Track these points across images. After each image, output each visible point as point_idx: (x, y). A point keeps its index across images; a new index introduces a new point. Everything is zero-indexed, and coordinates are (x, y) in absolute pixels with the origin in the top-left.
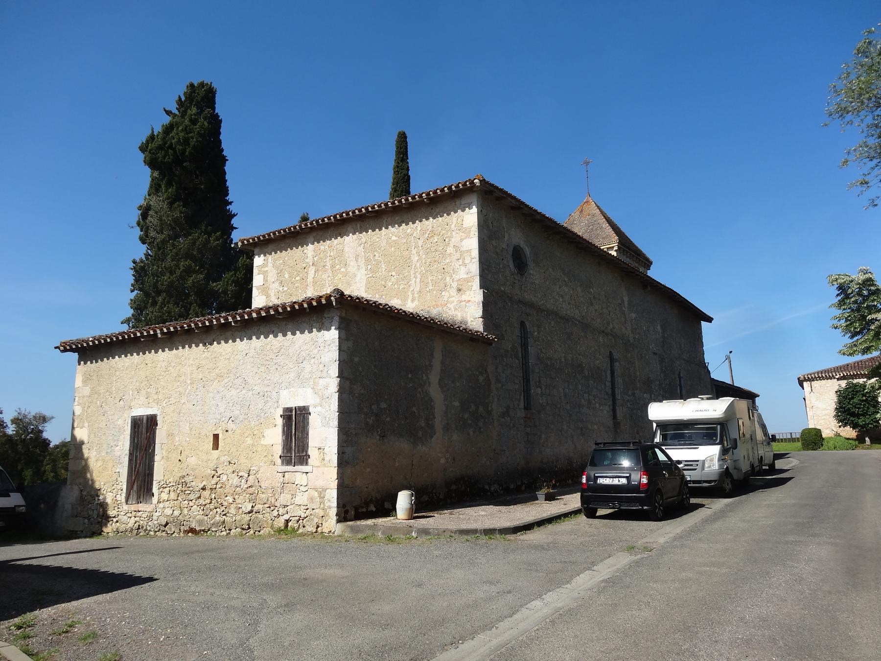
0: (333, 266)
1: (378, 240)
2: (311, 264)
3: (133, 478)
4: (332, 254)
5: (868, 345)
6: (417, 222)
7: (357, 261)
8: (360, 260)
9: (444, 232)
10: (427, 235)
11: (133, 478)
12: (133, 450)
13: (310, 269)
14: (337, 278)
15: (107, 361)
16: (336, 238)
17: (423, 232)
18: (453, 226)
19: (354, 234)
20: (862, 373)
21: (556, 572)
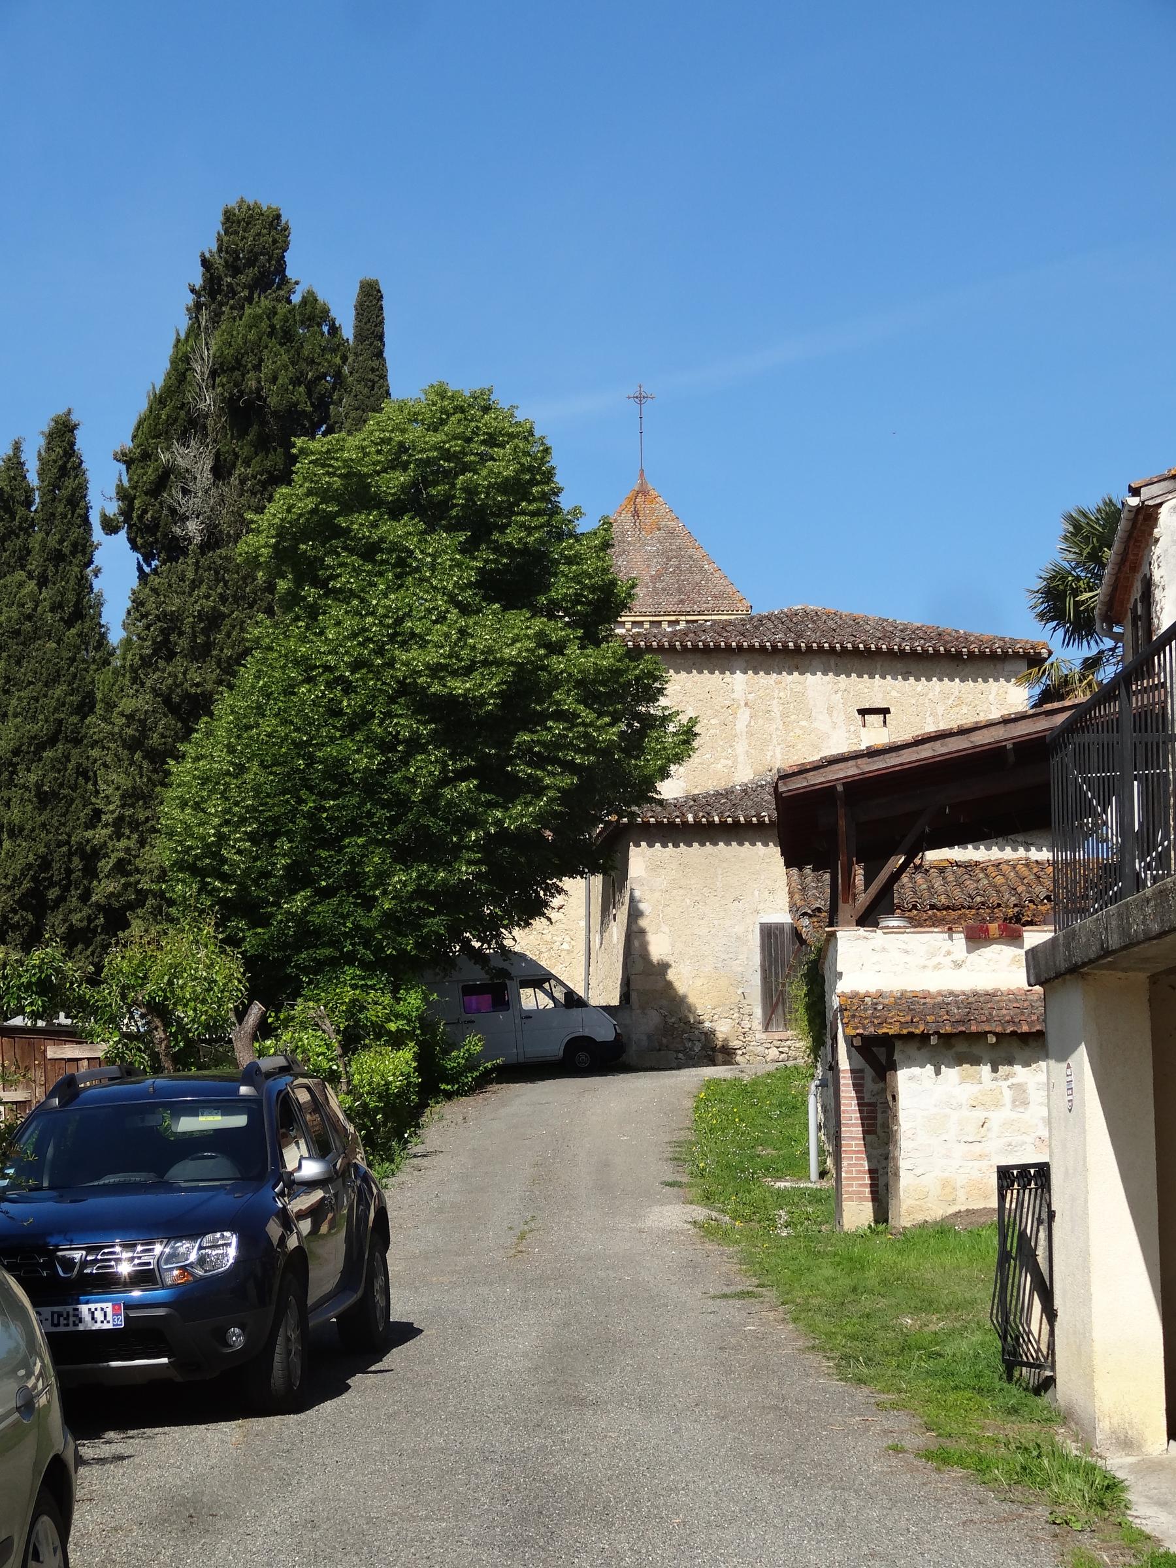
0: (785, 715)
1: (866, 690)
2: (742, 704)
3: (774, 1000)
4: (782, 694)
5: (218, 551)
6: (935, 679)
7: (830, 714)
8: (835, 714)
9: (977, 702)
10: (950, 702)
11: (774, 1000)
12: (770, 966)
13: (741, 711)
14: (792, 734)
15: (661, 848)
16: (790, 673)
17: (945, 696)
18: (991, 698)
19: (825, 673)
20: (195, 735)
21: (1050, 1146)
